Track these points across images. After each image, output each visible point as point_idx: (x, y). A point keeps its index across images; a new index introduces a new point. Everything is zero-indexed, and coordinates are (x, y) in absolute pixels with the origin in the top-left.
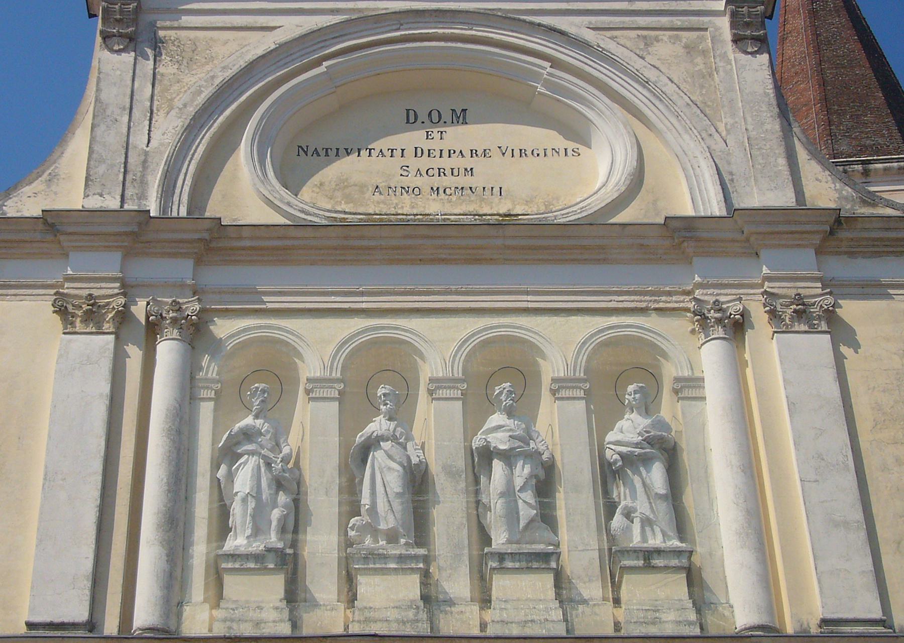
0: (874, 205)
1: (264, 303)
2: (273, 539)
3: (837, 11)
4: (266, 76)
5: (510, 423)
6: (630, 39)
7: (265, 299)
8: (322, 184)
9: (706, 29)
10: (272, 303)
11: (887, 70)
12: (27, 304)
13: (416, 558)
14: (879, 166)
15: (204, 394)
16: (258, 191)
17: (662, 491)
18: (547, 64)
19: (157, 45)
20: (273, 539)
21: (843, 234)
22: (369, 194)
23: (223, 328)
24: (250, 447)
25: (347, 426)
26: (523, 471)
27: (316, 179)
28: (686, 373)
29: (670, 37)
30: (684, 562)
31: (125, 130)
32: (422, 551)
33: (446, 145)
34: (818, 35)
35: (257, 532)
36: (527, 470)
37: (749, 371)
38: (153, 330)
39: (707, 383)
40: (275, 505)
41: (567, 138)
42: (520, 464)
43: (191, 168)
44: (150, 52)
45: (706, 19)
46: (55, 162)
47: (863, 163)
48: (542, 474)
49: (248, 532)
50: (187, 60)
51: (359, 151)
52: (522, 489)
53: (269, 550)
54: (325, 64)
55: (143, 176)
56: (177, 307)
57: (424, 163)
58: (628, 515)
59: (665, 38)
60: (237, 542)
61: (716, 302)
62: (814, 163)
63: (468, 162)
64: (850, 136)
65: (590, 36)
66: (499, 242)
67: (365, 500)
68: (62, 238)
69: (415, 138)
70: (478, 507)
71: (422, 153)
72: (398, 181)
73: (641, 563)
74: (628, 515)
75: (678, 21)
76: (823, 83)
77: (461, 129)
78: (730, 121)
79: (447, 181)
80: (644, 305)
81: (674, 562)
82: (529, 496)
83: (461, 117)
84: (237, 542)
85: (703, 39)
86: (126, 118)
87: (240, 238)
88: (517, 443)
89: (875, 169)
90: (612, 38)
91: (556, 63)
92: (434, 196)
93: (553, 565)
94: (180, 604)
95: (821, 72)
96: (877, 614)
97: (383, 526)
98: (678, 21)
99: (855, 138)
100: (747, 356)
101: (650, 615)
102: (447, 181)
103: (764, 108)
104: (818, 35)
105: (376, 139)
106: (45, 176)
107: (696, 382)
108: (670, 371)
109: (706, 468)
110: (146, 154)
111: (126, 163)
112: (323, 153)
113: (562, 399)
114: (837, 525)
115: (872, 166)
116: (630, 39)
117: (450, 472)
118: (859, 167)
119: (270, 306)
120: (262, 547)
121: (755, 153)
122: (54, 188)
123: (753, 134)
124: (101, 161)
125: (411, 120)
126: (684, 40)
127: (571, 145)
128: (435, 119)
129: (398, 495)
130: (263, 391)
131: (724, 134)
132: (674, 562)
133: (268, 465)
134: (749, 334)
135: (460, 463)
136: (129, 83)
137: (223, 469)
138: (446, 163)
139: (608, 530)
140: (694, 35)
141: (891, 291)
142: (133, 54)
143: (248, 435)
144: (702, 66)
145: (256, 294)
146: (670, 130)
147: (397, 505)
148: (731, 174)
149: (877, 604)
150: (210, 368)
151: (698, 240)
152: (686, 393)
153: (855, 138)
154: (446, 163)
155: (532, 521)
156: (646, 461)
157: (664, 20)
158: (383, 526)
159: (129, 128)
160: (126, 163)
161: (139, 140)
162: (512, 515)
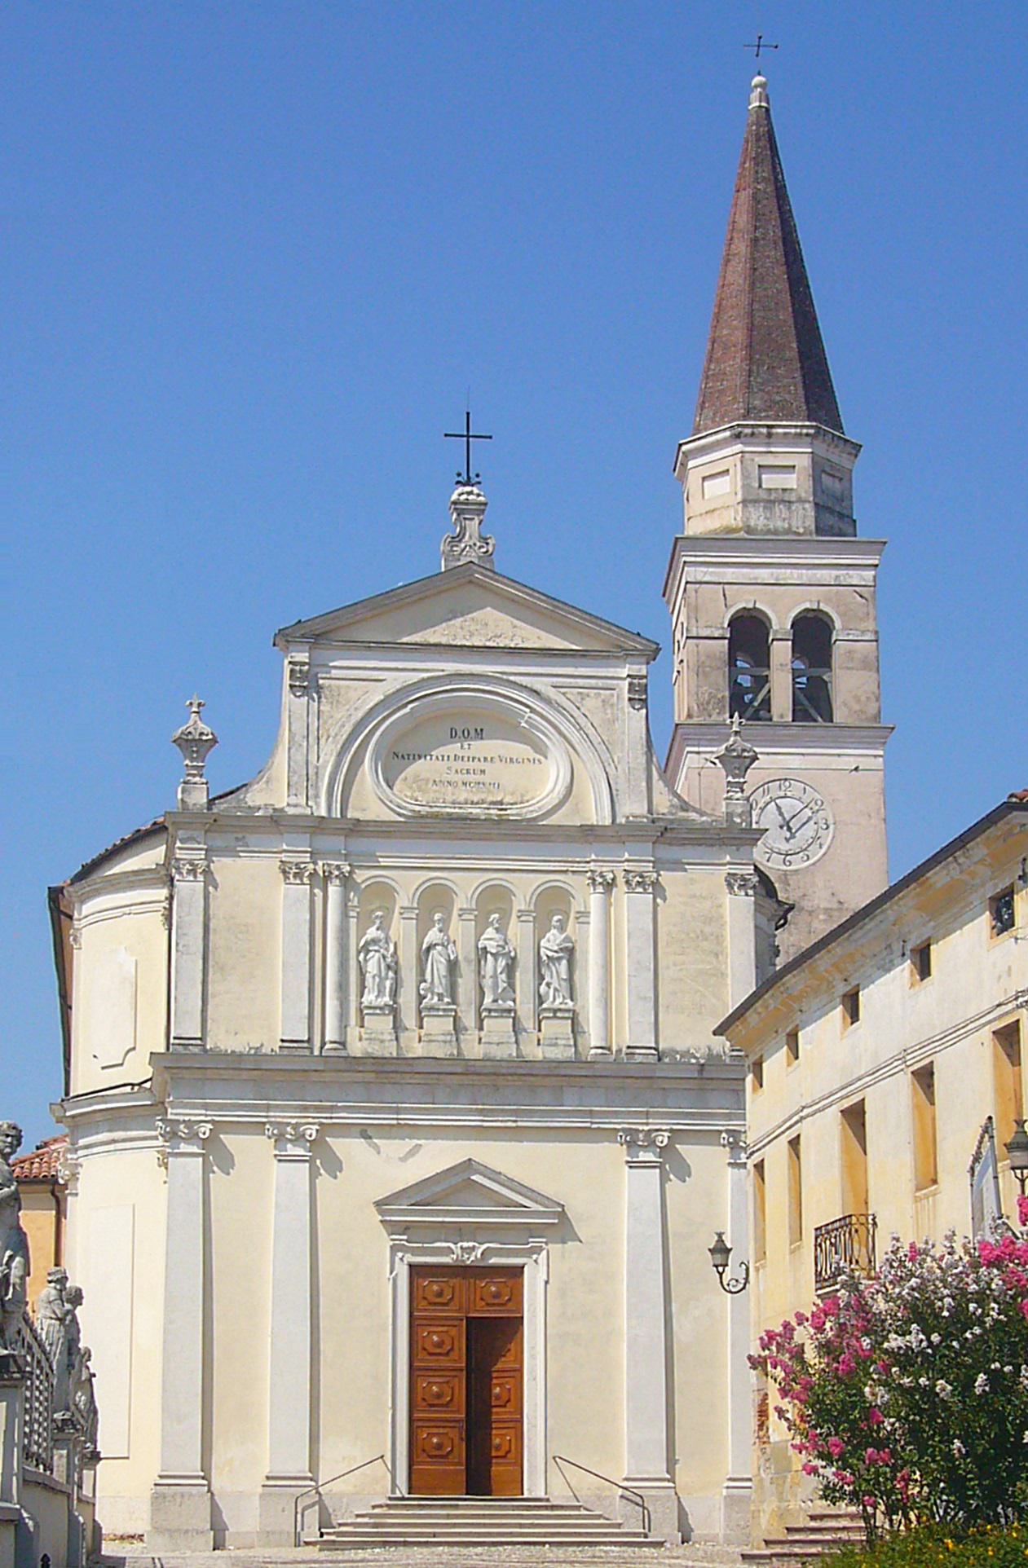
0: (687, 811)
1: (379, 862)
2: (387, 999)
3: (775, 243)
4: (378, 716)
5: (497, 936)
6: (572, 694)
7: (380, 859)
8: (406, 779)
9: (614, 689)
10: (383, 862)
11: (809, 312)
12: (265, 862)
13: (451, 1010)
14: (780, 431)
15: (352, 914)
16: (377, 795)
17: (565, 977)
18: (528, 710)
19: (319, 689)
20: (387, 999)
21: (668, 835)
22: (430, 785)
23: (360, 876)
24: (376, 948)
25: (421, 934)
26: (502, 962)
27: (402, 776)
28: (583, 909)
29: (595, 694)
30: (571, 1015)
31: (305, 752)
32: (454, 1007)
33: (471, 754)
34: (755, 269)
35: (380, 993)
36: (504, 963)
37: (612, 909)
38: (327, 878)
39: (592, 915)
40: (387, 978)
41: (536, 752)
42: (500, 959)
43: (341, 778)
44: (315, 695)
45: (615, 682)
46: (269, 769)
47: (768, 427)
48: (510, 962)
49: (376, 993)
50: (335, 703)
51: (425, 757)
52: (501, 973)
53: (386, 1005)
54: (411, 706)
55: (317, 783)
56: (338, 867)
57: (459, 765)
58: (548, 985)
59: (592, 695)
60: (369, 998)
61: (601, 873)
62: (661, 782)
63: (482, 766)
64: (763, 391)
65: (552, 693)
66: (497, 832)
67: (428, 976)
68: (281, 828)
69: (454, 748)
70: (479, 974)
71: (456, 734)
72: (445, 778)
73: (551, 1015)
74: (548, 985)
75: (600, 683)
76: (751, 328)
77: (479, 742)
78: (620, 755)
79: (471, 778)
80: (565, 869)
81: (566, 1015)
82: (504, 976)
83: (480, 734)
84: (369, 998)
85: (612, 695)
86: (305, 744)
87: (368, 826)
88: (500, 949)
89: (777, 433)
90: (564, 694)
91: (533, 710)
92: (464, 788)
93: (513, 1015)
94: (346, 1027)
95: (751, 315)
96: (653, 1045)
97: (436, 990)
98: (600, 683)
99: (768, 393)
100: (612, 900)
101: (554, 1041)
102: (471, 778)
103: (639, 747)
104: (755, 269)
105: (435, 749)
106: (264, 779)
107: (586, 914)
108: (576, 906)
109: (587, 961)
110: (317, 768)
111: (307, 774)
112: (406, 757)
113: (522, 921)
114: (641, 998)
115: (774, 431)
116: (572, 694)
117: (469, 962)
118: (764, 430)
119: (382, 864)
120: (383, 1003)
121: (631, 777)
122: (270, 786)
123: (631, 765)
124: (295, 773)
125: (453, 735)
126: (603, 697)
127: (538, 756)
128: (466, 736)
129: (444, 976)
130: (381, 917)
131: (616, 762)
132: (566, 1015)
133: (384, 957)
134: (615, 890)
135: (473, 956)
136: (305, 718)
137: (362, 955)
138: (471, 765)
139: (539, 991)
140: (608, 692)
141: (687, 867)
142: (306, 698)
143: (374, 941)
144: (609, 716)
145: (376, 858)
146: (559, 1067)
147: (443, 981)
148: (617, 790)
149: (653, 1039)
150: (354, 899)
151: (596, 836)
152: (581, 920)
153: (768, 393)
154: (471, 765)
155: (504, 989)
156: (559, 959)
157: (593, 682)
158: (436, 990)
159: (308, 750)
160: (307, 774)
161: (313, 758)
162: (496, 985)
